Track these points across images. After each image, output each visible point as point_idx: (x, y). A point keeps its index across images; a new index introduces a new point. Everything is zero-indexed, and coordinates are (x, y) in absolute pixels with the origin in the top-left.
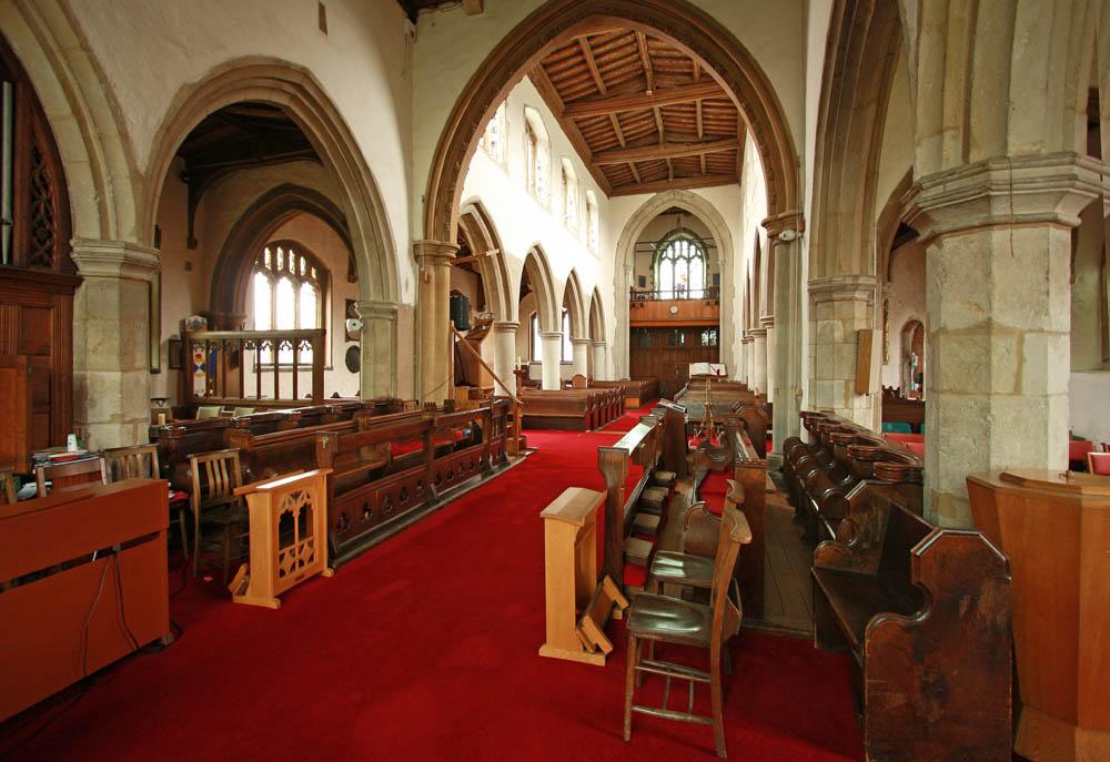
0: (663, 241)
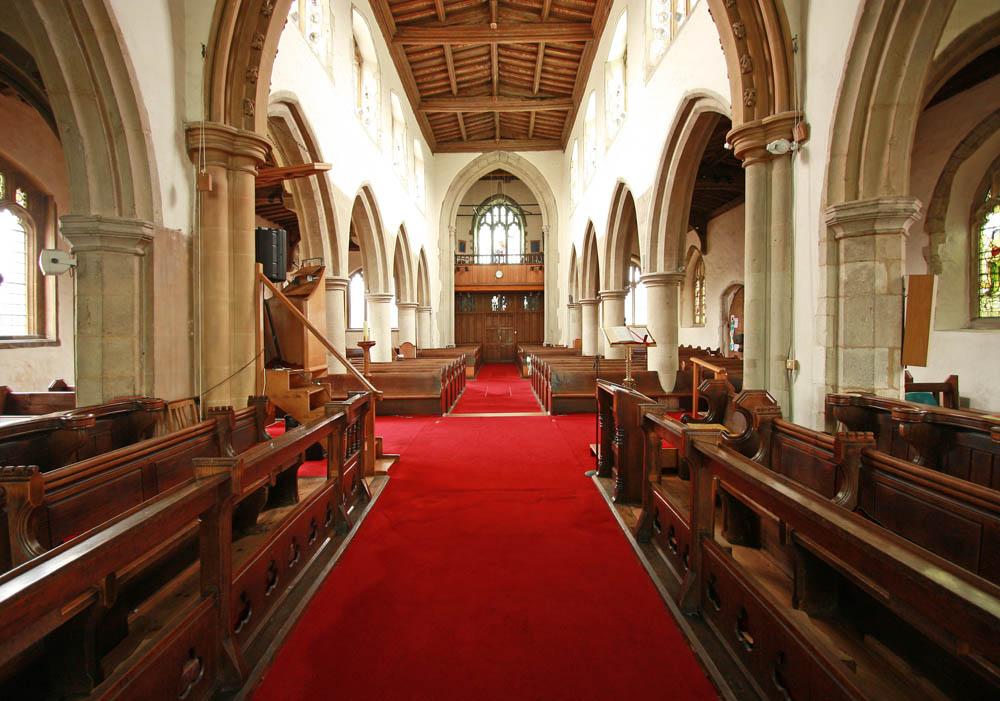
0: (482, 206)
